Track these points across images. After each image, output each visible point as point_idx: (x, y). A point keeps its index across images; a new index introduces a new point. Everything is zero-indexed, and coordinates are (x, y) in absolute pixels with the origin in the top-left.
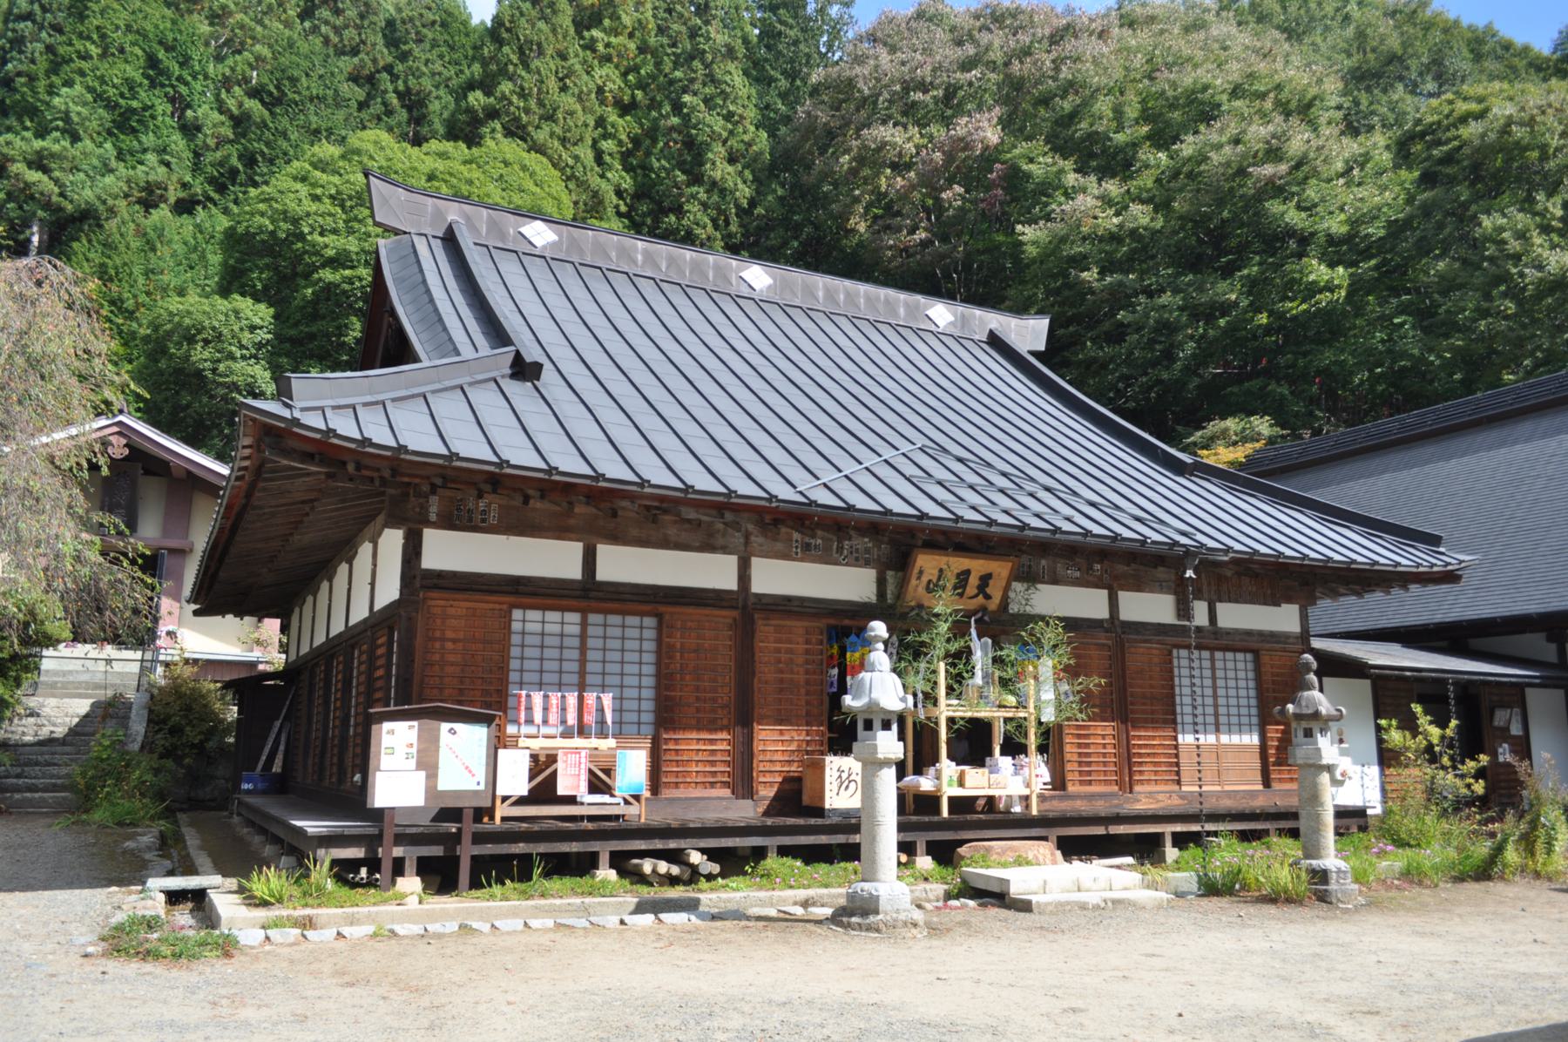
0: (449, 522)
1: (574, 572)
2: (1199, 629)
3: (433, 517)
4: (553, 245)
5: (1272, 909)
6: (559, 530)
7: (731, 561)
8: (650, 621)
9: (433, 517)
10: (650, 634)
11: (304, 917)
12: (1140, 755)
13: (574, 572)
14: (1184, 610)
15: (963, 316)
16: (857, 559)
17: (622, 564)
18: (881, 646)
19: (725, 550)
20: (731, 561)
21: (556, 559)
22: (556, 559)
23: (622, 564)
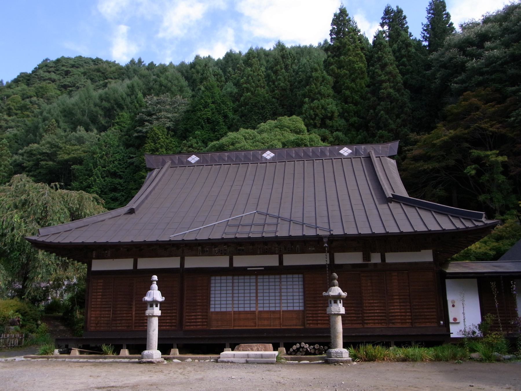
0: (98, 257)
1: (277, 264)
2: (375, 264)
3: (94, 256)
4: (273, 158)
5: (140, 365)
6: (222, 253)
7: (227, 258)
8: (301, 276)
9: (94, 256)
10: (301, 279)
11: (260, 354)
12: (367, 313)
13: (277, 264)
14: (366, 257)
15: (356, 149)
16: (221, 253)
17: (291, 260)
18: (155, 282)
19: (176, 256)
20: (227, 258)
21: (222, 262)
22: (222, 262)
23: (291, 260)
